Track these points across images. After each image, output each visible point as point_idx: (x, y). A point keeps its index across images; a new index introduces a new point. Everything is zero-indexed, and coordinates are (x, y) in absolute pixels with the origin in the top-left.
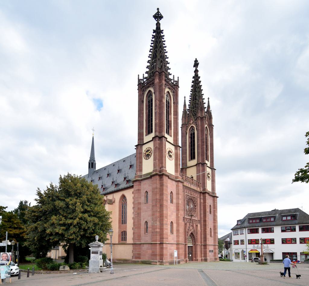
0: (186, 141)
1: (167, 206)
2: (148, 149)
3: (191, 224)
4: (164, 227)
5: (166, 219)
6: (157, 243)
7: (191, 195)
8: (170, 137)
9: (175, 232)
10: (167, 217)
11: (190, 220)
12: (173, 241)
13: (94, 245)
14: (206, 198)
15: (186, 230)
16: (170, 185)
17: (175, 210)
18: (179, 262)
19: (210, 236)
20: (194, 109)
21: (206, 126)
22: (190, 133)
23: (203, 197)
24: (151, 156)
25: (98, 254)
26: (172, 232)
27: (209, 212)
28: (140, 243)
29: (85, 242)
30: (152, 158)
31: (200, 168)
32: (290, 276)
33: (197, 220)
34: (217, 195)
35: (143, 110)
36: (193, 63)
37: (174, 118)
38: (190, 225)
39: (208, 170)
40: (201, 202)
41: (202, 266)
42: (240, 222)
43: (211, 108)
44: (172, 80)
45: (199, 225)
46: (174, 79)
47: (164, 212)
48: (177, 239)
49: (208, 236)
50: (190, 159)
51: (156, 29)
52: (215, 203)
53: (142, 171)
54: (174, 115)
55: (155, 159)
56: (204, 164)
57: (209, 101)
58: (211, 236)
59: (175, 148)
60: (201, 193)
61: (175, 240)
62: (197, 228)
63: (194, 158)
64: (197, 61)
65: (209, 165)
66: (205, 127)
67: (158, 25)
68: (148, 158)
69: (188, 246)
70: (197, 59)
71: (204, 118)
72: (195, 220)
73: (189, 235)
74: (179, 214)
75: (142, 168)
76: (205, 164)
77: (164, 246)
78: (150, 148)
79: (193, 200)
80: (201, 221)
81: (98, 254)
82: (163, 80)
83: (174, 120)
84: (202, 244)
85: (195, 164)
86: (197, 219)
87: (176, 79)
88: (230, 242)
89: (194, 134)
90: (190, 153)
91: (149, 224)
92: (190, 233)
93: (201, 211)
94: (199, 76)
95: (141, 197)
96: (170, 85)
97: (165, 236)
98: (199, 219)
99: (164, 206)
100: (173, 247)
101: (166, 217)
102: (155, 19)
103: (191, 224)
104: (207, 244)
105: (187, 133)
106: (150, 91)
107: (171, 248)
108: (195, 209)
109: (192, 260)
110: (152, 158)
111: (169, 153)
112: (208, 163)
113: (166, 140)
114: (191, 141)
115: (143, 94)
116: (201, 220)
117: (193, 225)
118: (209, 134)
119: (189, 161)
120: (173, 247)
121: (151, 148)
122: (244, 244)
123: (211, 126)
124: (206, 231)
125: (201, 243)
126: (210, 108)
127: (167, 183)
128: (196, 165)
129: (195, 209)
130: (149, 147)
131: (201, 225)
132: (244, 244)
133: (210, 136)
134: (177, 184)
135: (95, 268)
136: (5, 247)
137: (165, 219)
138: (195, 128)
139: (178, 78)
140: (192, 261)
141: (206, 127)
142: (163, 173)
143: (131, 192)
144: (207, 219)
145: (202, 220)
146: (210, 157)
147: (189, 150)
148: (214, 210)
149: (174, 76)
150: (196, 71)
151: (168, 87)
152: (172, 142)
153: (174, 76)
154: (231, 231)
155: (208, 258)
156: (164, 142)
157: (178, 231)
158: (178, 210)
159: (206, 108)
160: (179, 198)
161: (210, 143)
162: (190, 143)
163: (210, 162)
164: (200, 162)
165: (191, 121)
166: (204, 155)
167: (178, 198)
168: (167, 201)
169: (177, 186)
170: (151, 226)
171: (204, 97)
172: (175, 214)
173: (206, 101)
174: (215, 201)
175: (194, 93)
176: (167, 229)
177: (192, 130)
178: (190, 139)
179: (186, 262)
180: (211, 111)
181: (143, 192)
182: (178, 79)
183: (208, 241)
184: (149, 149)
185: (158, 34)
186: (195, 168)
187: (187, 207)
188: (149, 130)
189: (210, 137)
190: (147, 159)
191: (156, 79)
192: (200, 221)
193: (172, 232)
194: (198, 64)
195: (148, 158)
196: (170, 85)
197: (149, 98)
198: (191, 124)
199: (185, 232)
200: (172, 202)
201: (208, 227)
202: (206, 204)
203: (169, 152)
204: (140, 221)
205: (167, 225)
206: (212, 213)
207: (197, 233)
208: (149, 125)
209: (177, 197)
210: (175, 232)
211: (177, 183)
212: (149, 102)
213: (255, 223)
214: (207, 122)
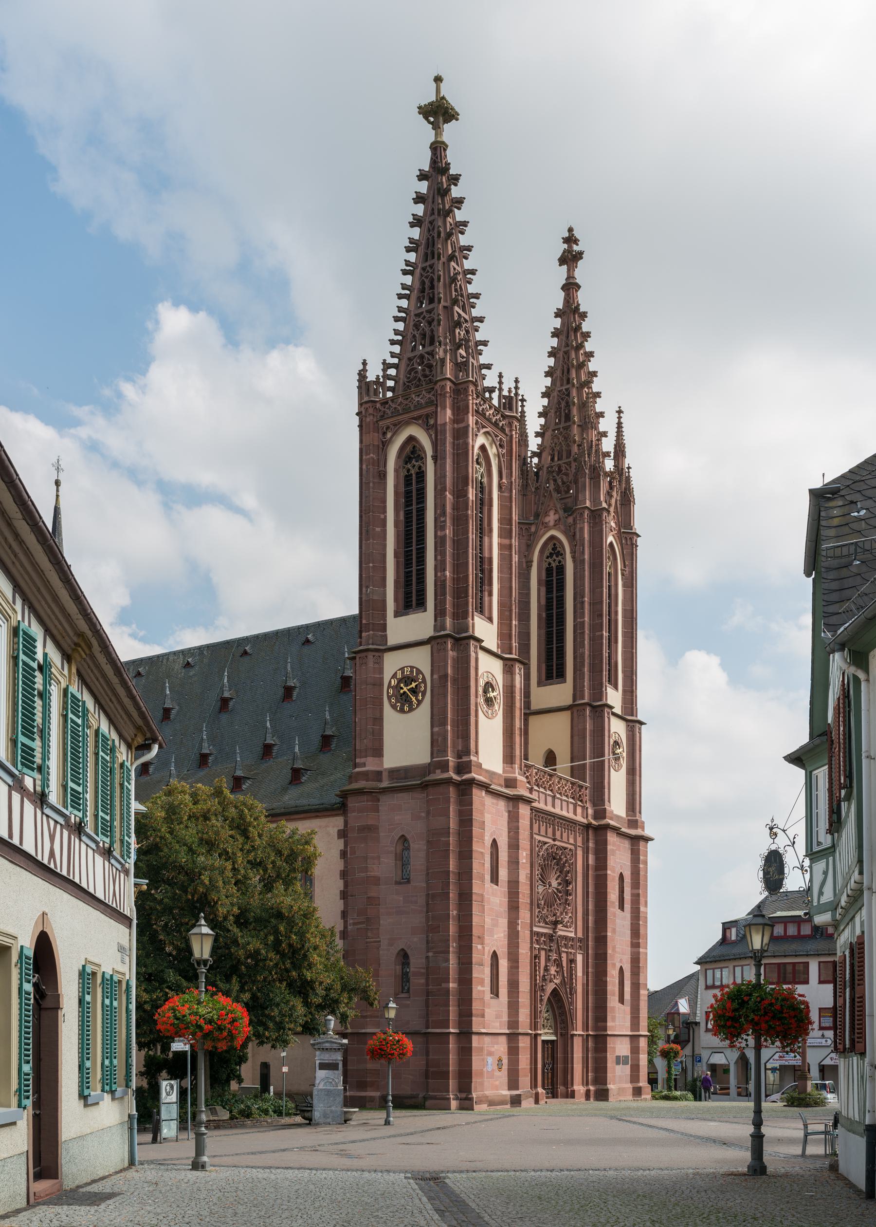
1: (482, 895)
2: (407, 672)
3: (554, 956)
4: (474, 976)
5: (480, 947)
6: (452, 1030)
7: (554, 840)
8: (489, 625)
9: (503, 990)
10: (481, 938)
11: (551, 940)
12: (498, 1024)
13: (327, 1045)
14: (609, 847)
15: (536, 980)
16: (490, 816)
17: (504, 908)
18: (516, 1101)
19: (617, 998)
22: (545, 565)
23: (596, 843)
24: (394, 676)
26: (495, 992)
27: (617, 904)
29: (296, 1034)
31: (585, 722)
33: (572, 939)
34: (648, 832)
35: (385, 508)
37: (501, 547)
38: (548, 959)
39: (617, 728)
40: (588, 865)
41: (702, 1103)
42: (734, 930)
45: (579, 958)
46: (501, 390)
47: (475, 920)
48: (509, 1016)
49: (612, 1001)
51: (431, 166)
52: (641, 866)
54: (500, 536)
56: (600, 710)
57: (619, 426)
58: (622, 1000)
59: (505, 666)
60: (588, 826)
61: (505, 1018)
62: (572, 971)
64: (576, 241)
66: (608, 542)
67: (438, 149)
68: (406, 708)
69: (543, 1041)
71: (605, 514)
72: (566, 938)
73: (545, 998)
76: (606, 709)
77: (475, 1041)
78: (417, 669)
79: (561, 859)
80: (588, 940)
81: (337, 1069)
82: (468, 412)
83: (501, 556)
84: (591, 1033)
86: (572, 935)
88: (691, 1019)
89: (561, 569)
91: (416, 963)
92: (550, 987)
93: (588, 902)
94: (452, 172)
95: (379, 858)
96: (489, 420)
97: (476, 1006)
98: (580, 935)
99: (474, 897)
100: (497, 1044)
101: (479, 937)
102: (426, 118)
103: (554, 956)
104: (609, 1033)
105: (532, 561)
107: (493, 1049)
108: (568, 893)
109: (552, 1093)
111: (485, 692)
112: (614, 697)
114: (549, 600)
115: (385, 445)
116: (588, 936)
117: (560, 957)
121: (419, 672)
123: (628, 537)
124: (606, 981)
125: (587, 1030)
127: (482, 814)
129: (568, 893)
130: (412, 667)
131: (588, 959)
134: (511, 809)
135: (332, 1111)
136: (187, 1051)
137: (477, 947)
138: (564, 549)
139: (517, 381)
140: (553, 1097)
142: (473, 779)
143: (334, 832)
144: (609, 934)
145: (591, 935)
146: (623, 672)
147: (539, 636)
148: (632, 895)
149: (500, 376)
150: (570, 287)
151: (485, 430)
153: (500, 376)
154: (698, 967)
155: (610, 1086)
157: (513, 985)
158: (513, 907)
159: (607, 454)
161: (624, 610)
162: (544, 608)
163: (624, 691)
164: (586, 701)
165: (552, 513)
166: (602, 671)
168: (482, 879)
169: (513, 818)
170: (423, 971)
171: (600, 406)
172: (503, 922)
173: (607, 424)
174: (641, 858)
175: (564, 388)
176: (482, 982)
177: (551, 555)
178: (543, 589)
179: (537, 1101)
180: (629, 468)
181: (387, 840)
183: (614, 1020)
184: (412, 672)
186: (565, 717)
187: (541, 889)
188: (408, 596)
189: (624, 586)
190: (402, 711)
191: (444, 408)
192: (584, 941)
193: (495, 992)
194: (579, 256)
195: (406, 708)
196: (489, 420)
197: (409, 466)
198: (547, 528)
199: (536, 989)
200: (495, 879)
201: (614, 965)
202: (609, 872)
203: (489, 686)
204: (378, 948)
205: (482, 965)
206: (627, 906)
207: (573, 992)
208: (408, 575)
209: (509, 857)
210: (503, 990)
211: (511, 804)
213: (793, 937)
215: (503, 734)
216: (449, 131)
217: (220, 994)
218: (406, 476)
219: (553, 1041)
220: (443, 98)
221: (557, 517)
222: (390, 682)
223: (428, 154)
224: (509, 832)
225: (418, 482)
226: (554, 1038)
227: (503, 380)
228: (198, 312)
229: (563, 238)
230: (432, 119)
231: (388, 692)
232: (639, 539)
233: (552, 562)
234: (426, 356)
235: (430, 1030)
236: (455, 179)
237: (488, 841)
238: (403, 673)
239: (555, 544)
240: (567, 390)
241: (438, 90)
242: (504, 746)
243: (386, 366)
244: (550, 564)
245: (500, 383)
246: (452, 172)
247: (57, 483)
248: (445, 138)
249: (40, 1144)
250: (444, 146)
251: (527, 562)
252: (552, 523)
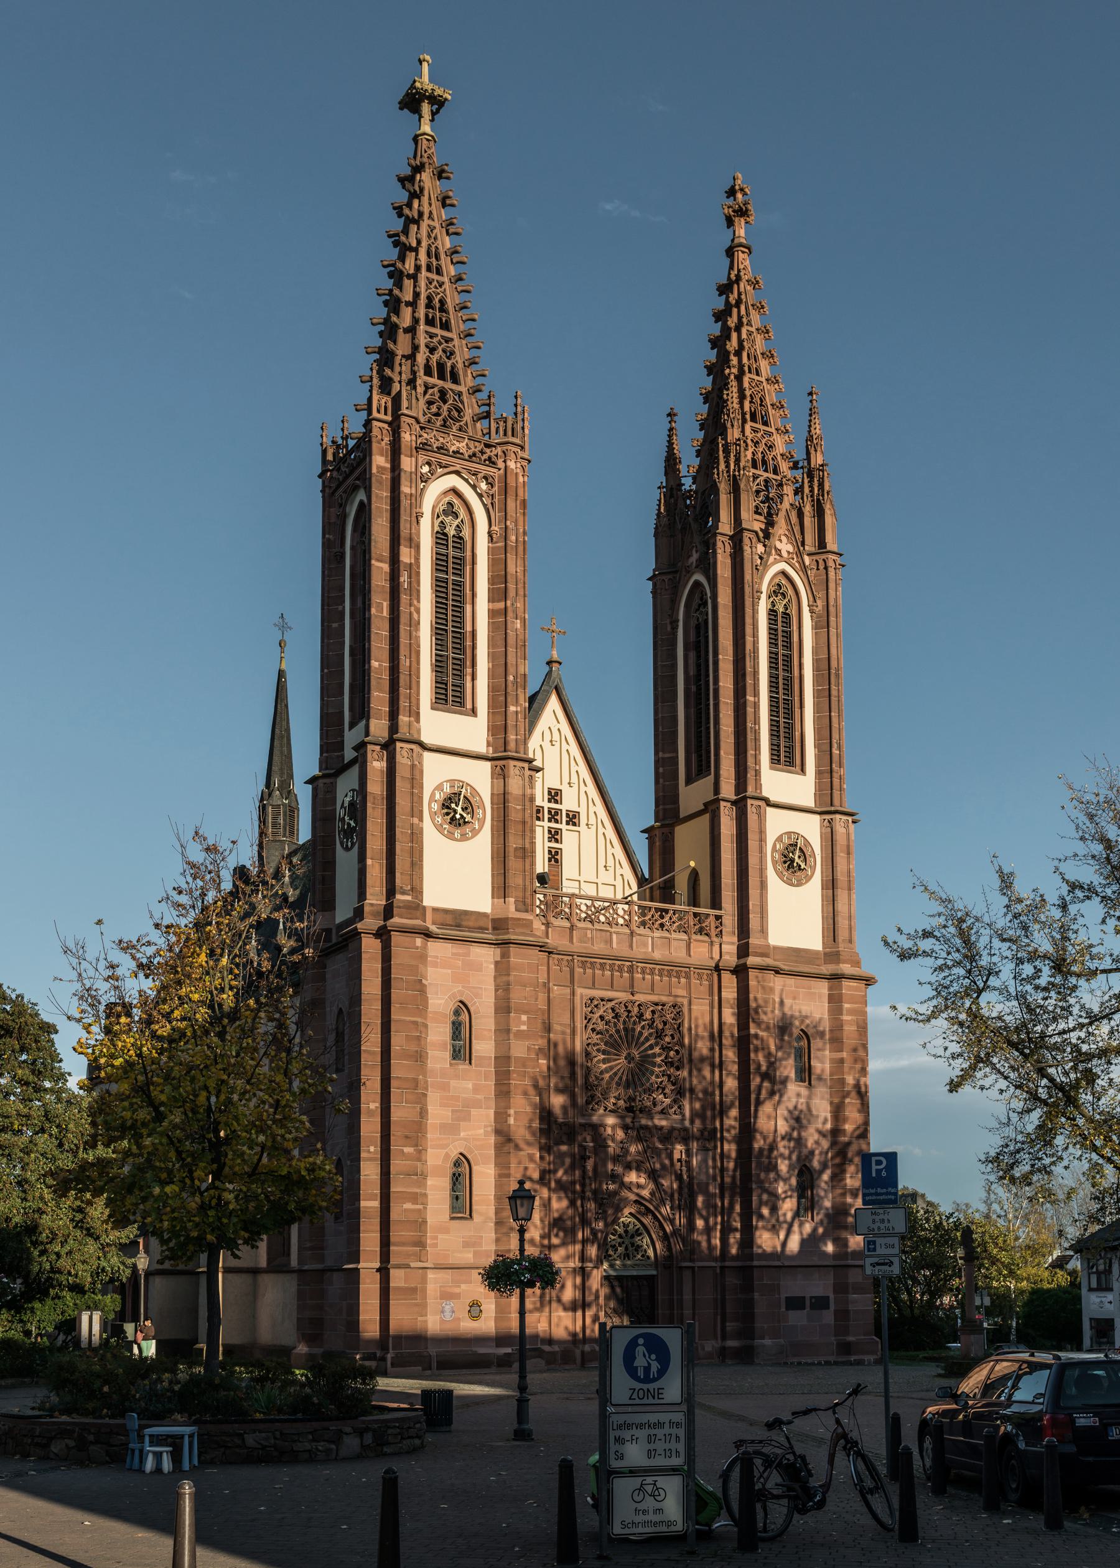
0: (674, 666)
5: (408, 1150)
25: (828, 1308)
28: (319, 1266)
32: (566, 1470)
37: (492, 613)
53: (334, 909)
54: (491, 600)
68: (457, 835)
74: (512, 1112)
75: (333, 889)
78: (792, 885)
83: (493, 627)
105: (678, 621)
106: (697, 584)
120: (463, 1286)
122: (1091, 1319)
132: (1091, 1319)
158: (503, 1092)
160: (508, 1031)
161: (816, 662)
163: (819, 773)
167: (503, 1032)
185: (281, 674)
209: (497, 1023)
212: (698, 627)
215: (492, 858)
217: (787, 1162)
219: (653, 1276)
224: (496, 990)
226: (654, 1273)
228: (702, 427)
234: (427, 396)
235: (306, 1267)
237: (335, 1010)
242: (493, 875)
247: (281, 644)
251: (671, 623)
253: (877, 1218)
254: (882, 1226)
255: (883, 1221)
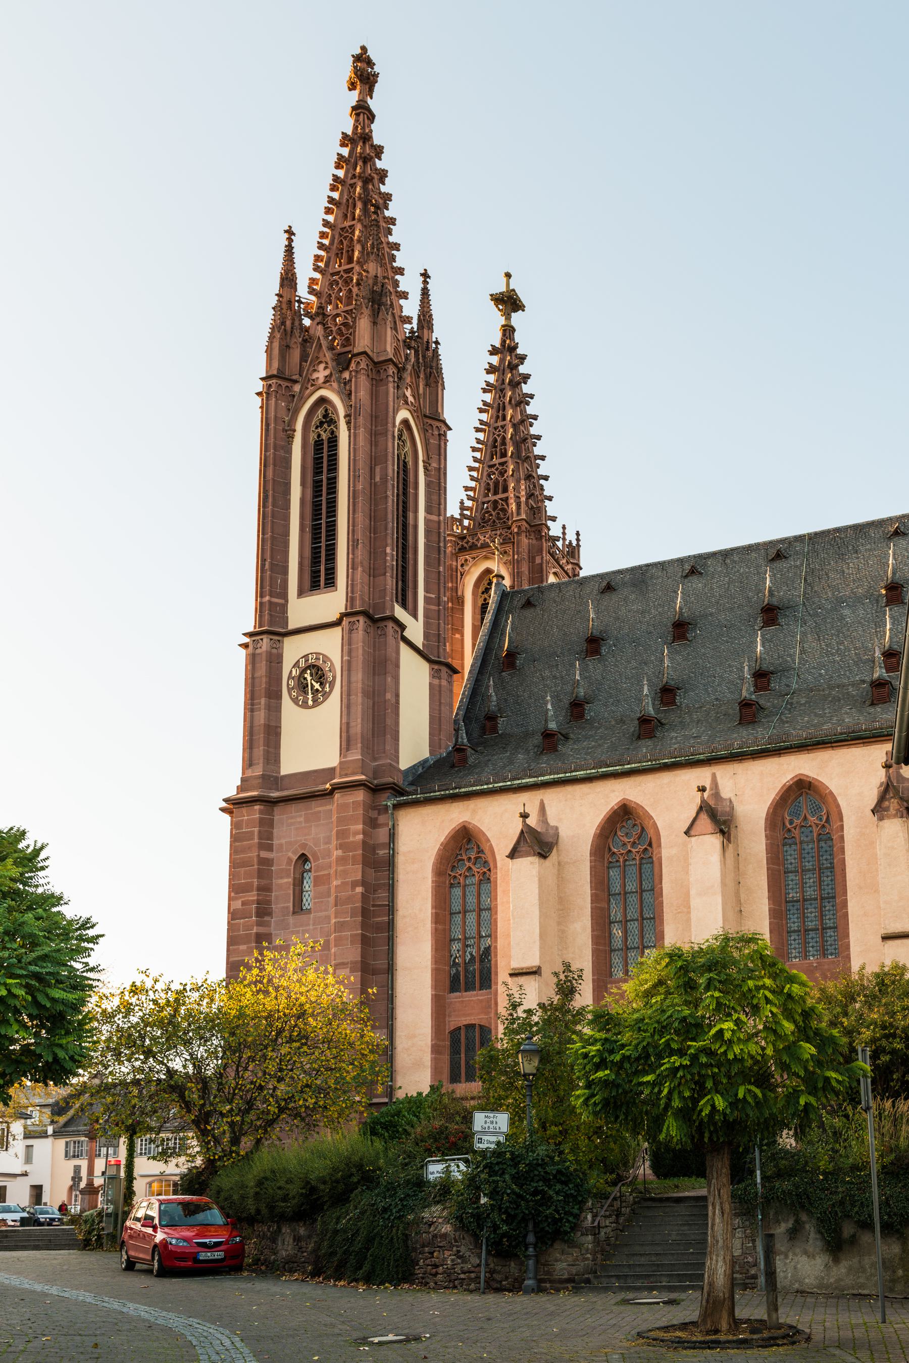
20: (496, 493)
21: (403, 414)
22: (312, 437)
24: (296, 665)
30: (333, 704)
36: (346, 70)
43: (439, 332)
44: (558, 541)
46: (564, 539)
50: (307, 583)
55: (347, 707)
57: (425, 293)
63: (331, 582)
65: (415, 630)
67: (508, 331)
70: (370, 53)
85: (334, 617)
87: (571, 537)
89: (333, 441)
90: (308, 553)
94: (519, 351)
110: (333, 704)
113: (402, 632)
118: (421, 464)
119: (301, 593)
126: (430, 328)
128: (337, 623)
133: (426, 475)
139: (578, 534)
141: (405, 422)
149: (564, 527)
150: (363, 112)
152: (419, 641)
153: (564, 527)
156: (391, 641)
159: (408, 320)
173: (409, 283)
177: (322, 423)
182: (578, 540)
190: (305, 705)
214: (408, 393)
216: (517, 319)
218: (483, 604)
220: (514, 290)
221: (327, 372)
222: (291, 671)
223: (499, 335)
225: (329, 471)
227: (566, 531)
229: (353, 56)
230: (501, 307)
231: (288, 684)
232: (449, 433)
233: (322, 433)
236: (522, 358)
238: (307, 661)
239: (326, 410)
240: (350, 227)
241: (508, 284)
243: (463, 507)
244: (319, 436)
245: (564, 533)
246: (519, 351)
248: (514, 322)
249: (53, 1151)
250: (513, 330)
252: (321, 380)
253: (488, 1120)
254: (491, 1126)
255: (492, 1123)
